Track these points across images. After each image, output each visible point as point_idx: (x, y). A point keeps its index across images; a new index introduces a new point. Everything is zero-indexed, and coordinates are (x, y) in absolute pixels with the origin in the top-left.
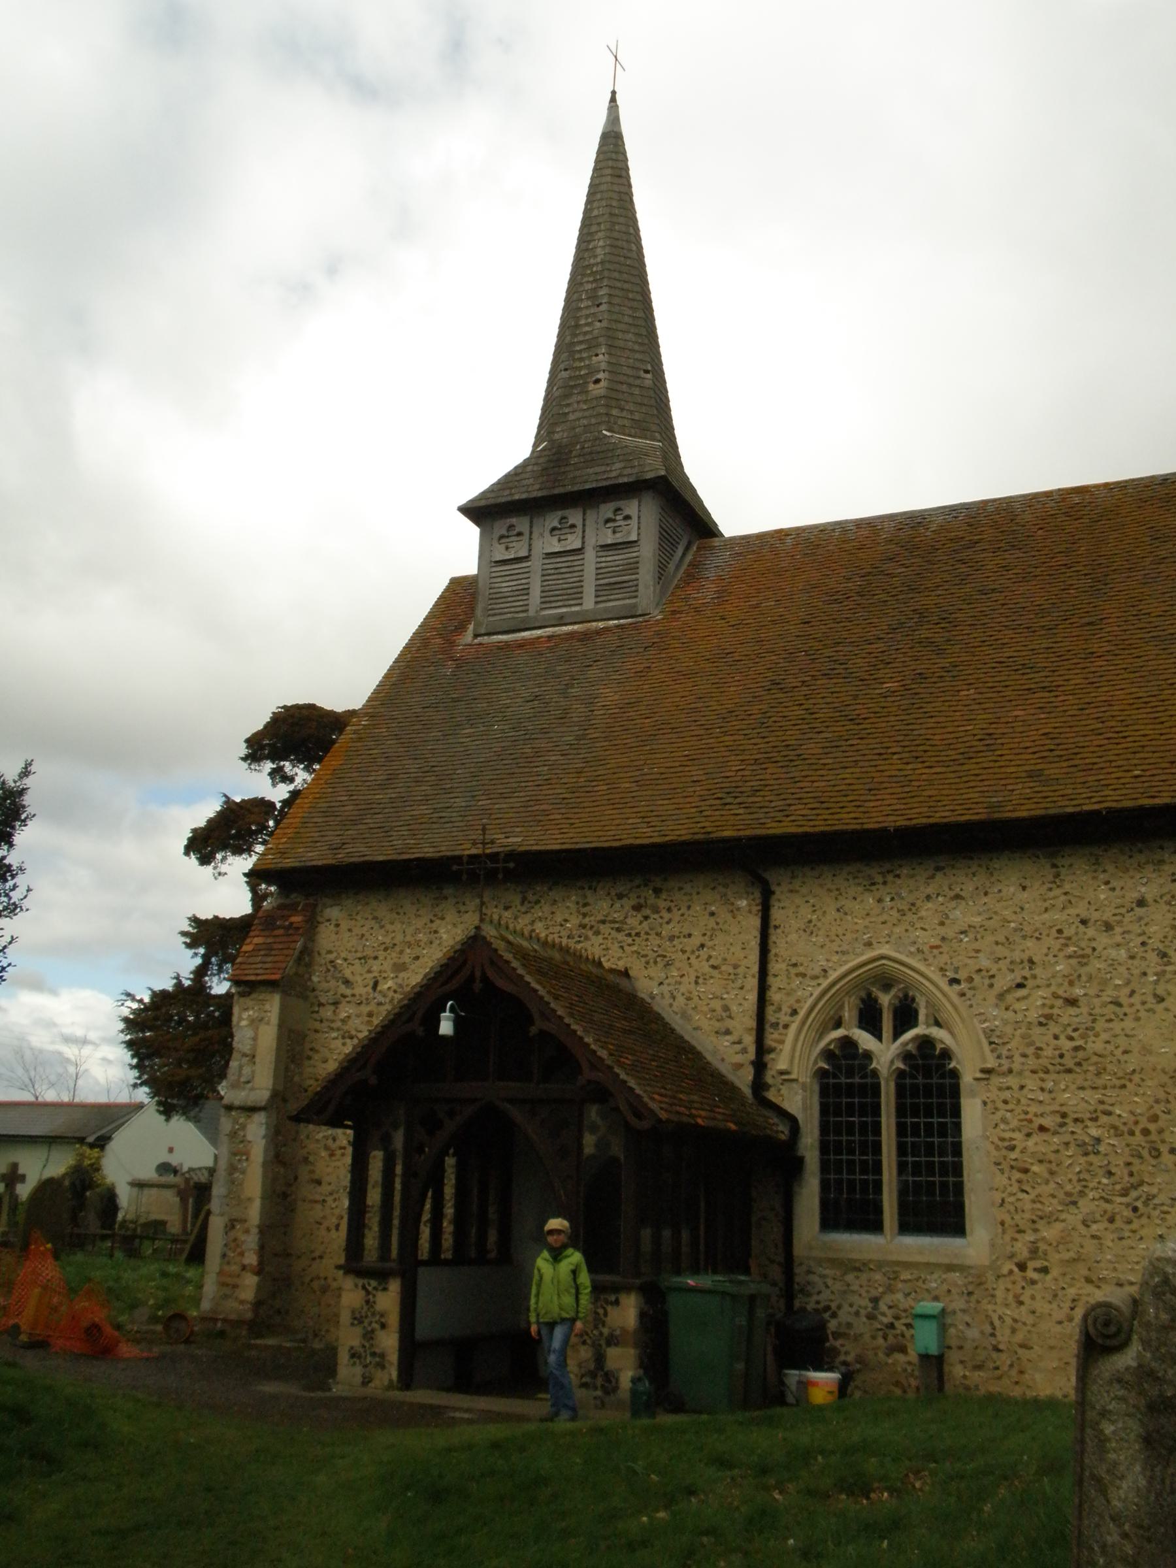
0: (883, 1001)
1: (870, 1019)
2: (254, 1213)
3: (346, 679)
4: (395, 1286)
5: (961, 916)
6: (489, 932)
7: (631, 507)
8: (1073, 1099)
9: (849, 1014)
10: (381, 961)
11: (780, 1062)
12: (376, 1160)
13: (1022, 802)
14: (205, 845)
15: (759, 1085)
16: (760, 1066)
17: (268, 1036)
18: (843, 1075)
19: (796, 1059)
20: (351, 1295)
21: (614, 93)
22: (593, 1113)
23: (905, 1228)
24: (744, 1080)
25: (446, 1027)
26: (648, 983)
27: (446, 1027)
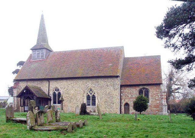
0: (57, 90)
1: (56, 90)
2: (16, 103)
3: (25, 59)
4: (23, 107)
5: (61, 84)
6: (28, 85)
7: (43, 50)
8: (68, 96)
9: (55, 90)
10: (23, 85)
11: (50, 93)
12: (22, 100)
13: (65, 77)
14: (14, 73)
15: (49, 95)
16: (49, 93)
17: (16, 91)
18: (54, 94)
19: (51, 93)
20: (21, 108)
21: (42, 15)
22: (34, 96)
23: (58, 104)
24: (48, 94)
25: (25, 92)
26: (42, 88)
27: (25, 92)
